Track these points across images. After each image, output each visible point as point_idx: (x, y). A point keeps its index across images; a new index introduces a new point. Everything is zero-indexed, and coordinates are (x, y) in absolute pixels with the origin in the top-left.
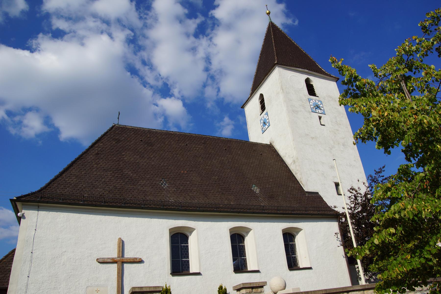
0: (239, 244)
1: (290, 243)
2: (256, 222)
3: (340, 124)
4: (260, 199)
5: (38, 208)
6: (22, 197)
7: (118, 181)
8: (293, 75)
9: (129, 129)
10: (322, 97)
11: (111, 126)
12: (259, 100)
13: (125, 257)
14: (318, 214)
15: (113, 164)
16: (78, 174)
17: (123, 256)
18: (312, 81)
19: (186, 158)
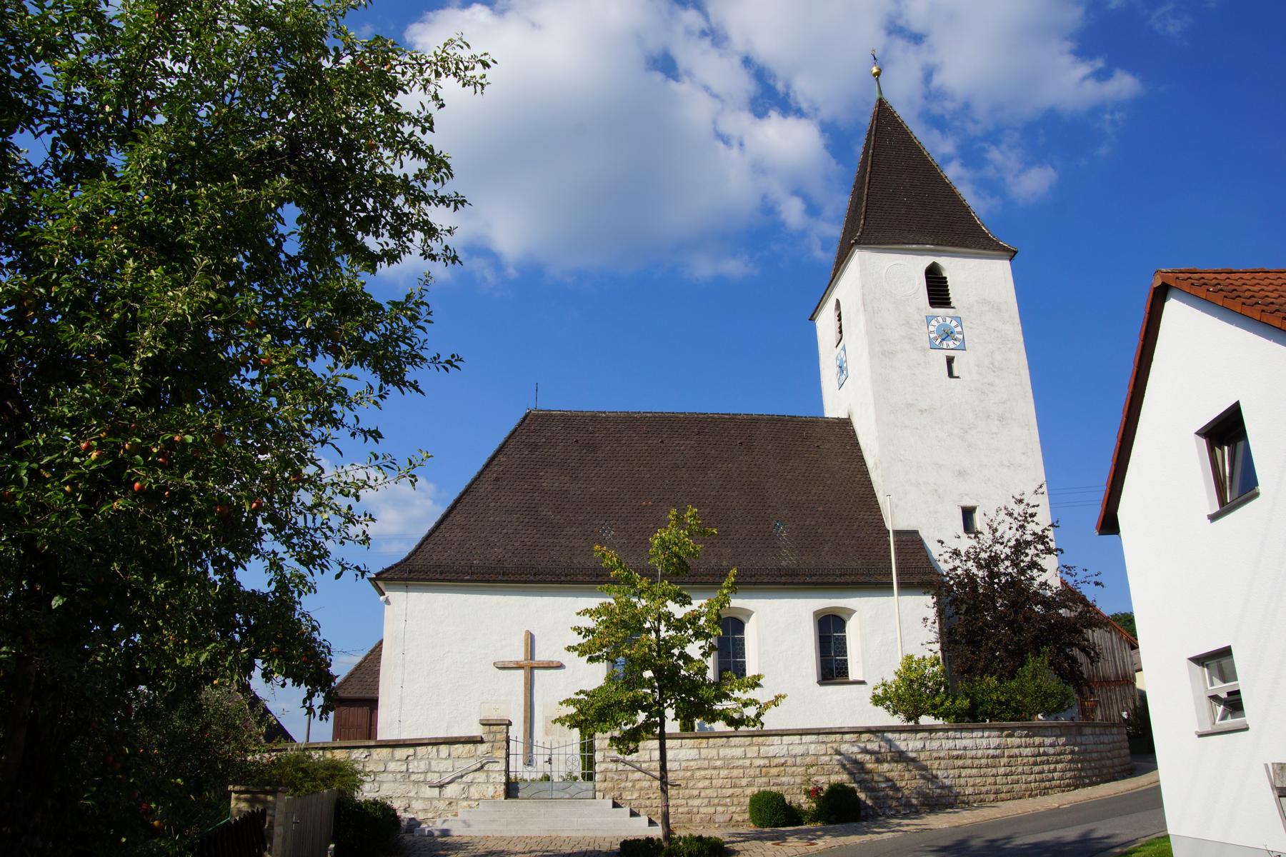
5: (407, 589)
6: (382, 573)
7: (529, 532)
8: (897, 262)
9: (555, 416)
11: (523, 415)
13: (536, 659)
14: (853, 583)
15: (522, 498)
16: (465, 523)
17: (532, 658)
19: (656, 472)
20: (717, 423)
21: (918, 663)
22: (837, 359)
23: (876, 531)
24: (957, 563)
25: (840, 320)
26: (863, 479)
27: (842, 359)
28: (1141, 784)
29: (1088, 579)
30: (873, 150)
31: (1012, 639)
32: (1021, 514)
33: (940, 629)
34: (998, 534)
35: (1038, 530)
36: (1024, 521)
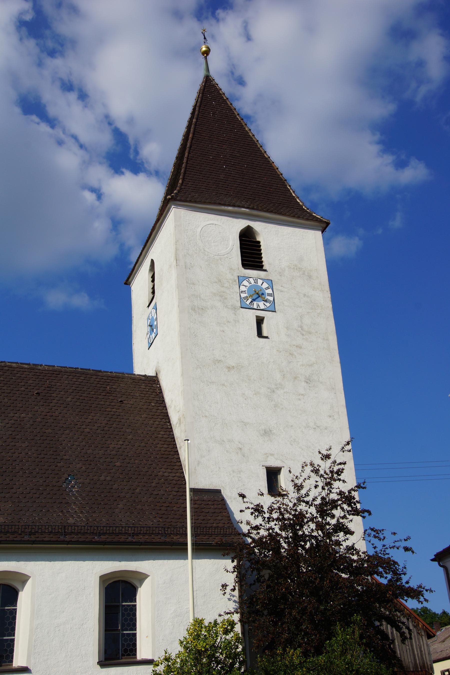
0: (4, 608)
1: (123, 604)
2: (41, 561)
3: (310, 333)
4: (72, 509)
8: (211, 222)
10: (276, 271)
12: (149, 274)
14: (146, 543)
18: (259, 234)
20: (15, 372)
21: (209, 629)
22: (148, 319)
23: (176, 489)
24: (259, 521)
25: (153, 281)
26: (165, 436)
27: (153, 318)
29: (397, 544)
30: (197, 119)
31: (318, 608)
32: (328, 471)
33: (240, 596)
34: (303, 492)
35: (345, 488)
36: (330, 478)
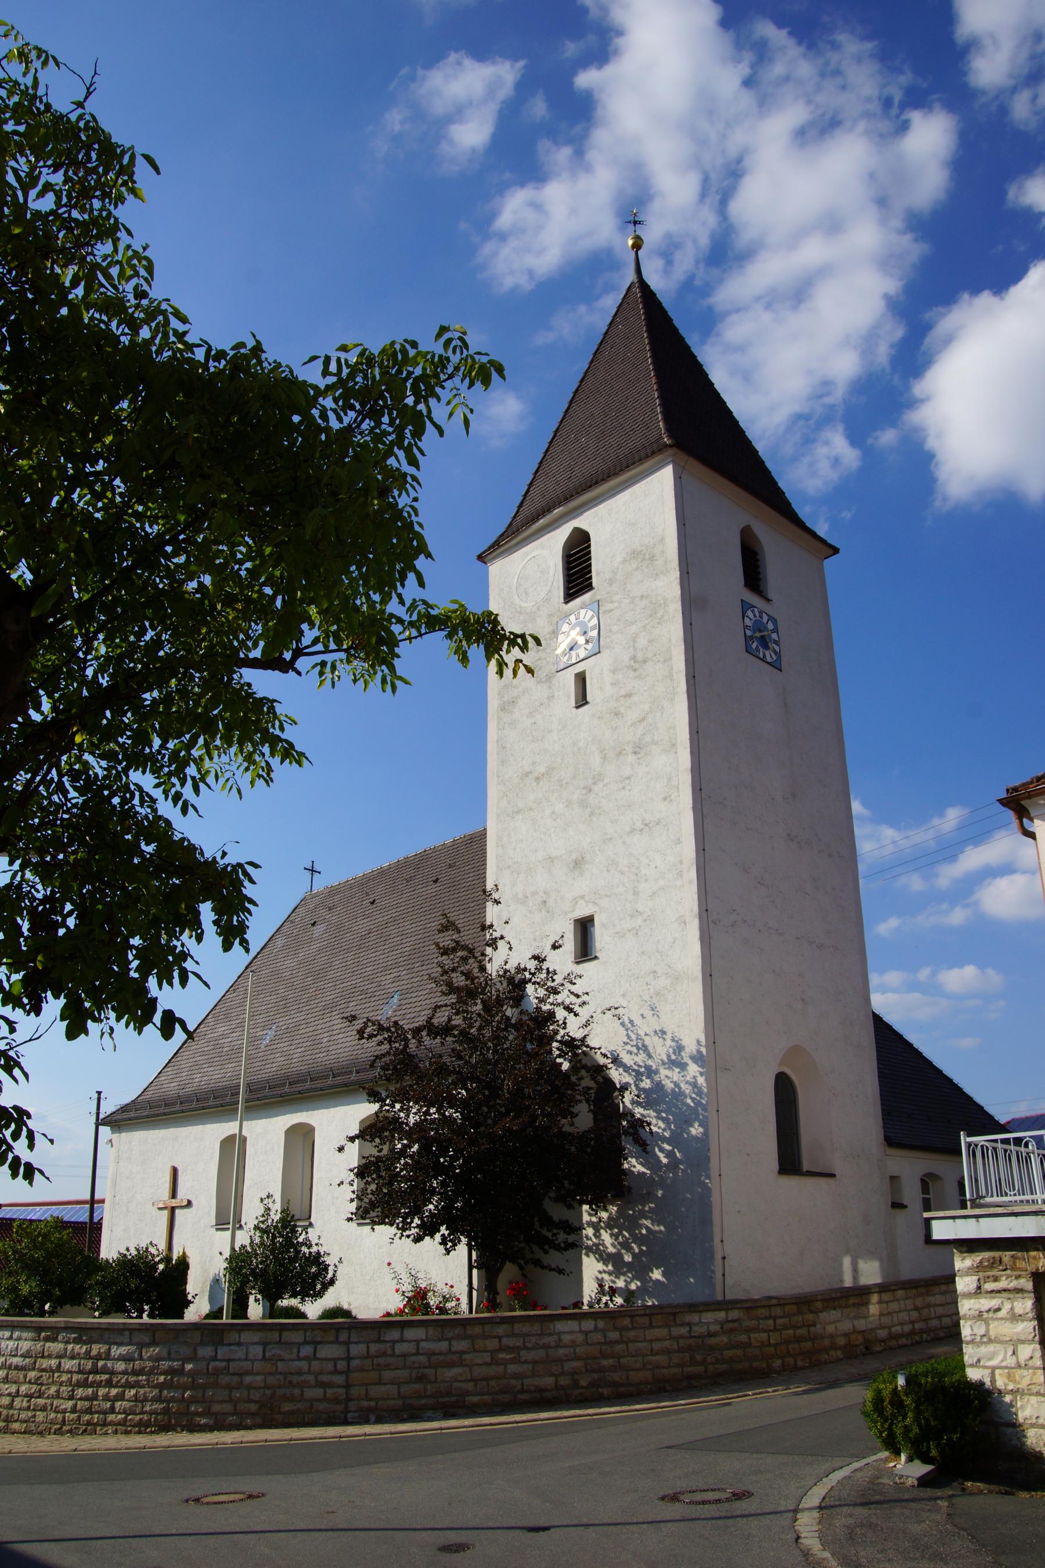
28: (222, 1440)
